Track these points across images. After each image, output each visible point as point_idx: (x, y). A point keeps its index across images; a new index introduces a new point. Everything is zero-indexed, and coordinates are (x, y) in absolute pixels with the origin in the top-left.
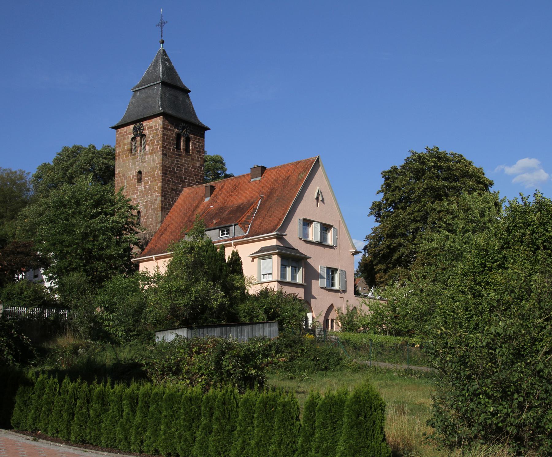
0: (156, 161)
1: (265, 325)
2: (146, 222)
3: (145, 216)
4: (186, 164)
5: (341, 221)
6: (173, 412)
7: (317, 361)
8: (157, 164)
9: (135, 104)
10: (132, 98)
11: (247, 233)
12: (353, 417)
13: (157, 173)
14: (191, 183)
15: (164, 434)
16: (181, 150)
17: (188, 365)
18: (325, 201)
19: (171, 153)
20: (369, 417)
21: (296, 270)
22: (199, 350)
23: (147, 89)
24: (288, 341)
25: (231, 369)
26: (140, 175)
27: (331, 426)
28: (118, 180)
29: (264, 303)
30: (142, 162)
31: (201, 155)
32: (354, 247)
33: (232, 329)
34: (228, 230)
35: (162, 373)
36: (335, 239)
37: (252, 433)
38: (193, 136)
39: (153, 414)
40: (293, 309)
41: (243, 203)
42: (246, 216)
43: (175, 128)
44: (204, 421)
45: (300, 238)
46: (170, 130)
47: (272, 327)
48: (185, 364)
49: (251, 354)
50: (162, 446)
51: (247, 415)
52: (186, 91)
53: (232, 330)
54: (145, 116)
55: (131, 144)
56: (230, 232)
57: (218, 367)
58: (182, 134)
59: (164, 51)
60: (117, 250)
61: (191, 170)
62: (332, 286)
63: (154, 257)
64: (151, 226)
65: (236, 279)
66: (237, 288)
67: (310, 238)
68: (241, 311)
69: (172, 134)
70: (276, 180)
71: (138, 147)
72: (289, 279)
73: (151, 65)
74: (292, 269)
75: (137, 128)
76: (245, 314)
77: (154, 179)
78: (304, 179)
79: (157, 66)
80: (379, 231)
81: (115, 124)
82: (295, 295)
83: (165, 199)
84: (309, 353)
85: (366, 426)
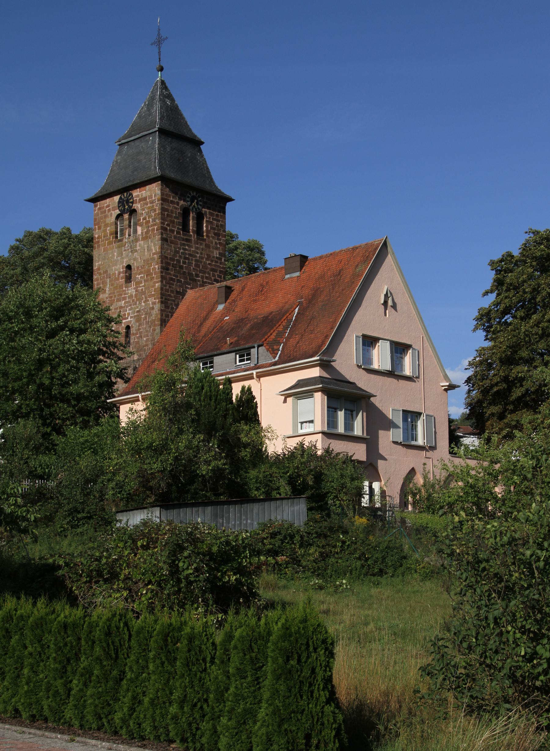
0: (152, 250)
1: (285, 502)
2: (138, 343)
3: (136, 334)
4: (198, 253)
5: (425, 338)
6: (42, 646)
7: (367, 560)
8: (154, 254)
9: (122, 164)
10: (117, 156)
11: (277, 359)
12: (280, 660)
13: (154, 269)
14: (206, 283)
15: (27, 683)
16: (189, 232)
17: (128, 566)
18: (398, 308)
19: (175, 237)
20: (306, 662)
21: (352, 415)
22: (148, 544)
23: (139, 140)
24: (321, 527)
25: (191, 574)
26: (129, 271)
27: (252, 676)
28: (97, 280)
29: (288, 467)
30: (132, 251)
31: (220, 240)
32: (446, 378)
33: (232, 508)
34: (249, 354)
35: (88, 579)
36: (417, 366)
37: (147, 684)
38: (208, 211)
39: (14, 650)
40: (342, 476)
41: (272, 312)
42: (276, 332)
43: (180, 199)
44: (84, 663)
45: (358, 366)
46: (172, 202)
47: (297, 505)
48: (124, 565)
49: (232, 548)
50: (23, 704)
51: (140, 653)
52: (197, 143)
53: (231, 510)
54: (135, 182)
55: (116, 224)
56: (252, 356)
57: (174, 570)
58: (191, 208)
59: (163, 82)
60: (88, 386)
61: (205, 263)
62: (412, 440)
63: (140, 396)
64: (146, 348)
65: (243, 430)
66: (246, 446)
67: (375, 366)
68: (251, 479)
69: (176, 208)
70: (322, 277)
71: (126, 229)
72: (341, 429)
73: (145, 105)
74: (345, 413)
75: (124, 201)
76: (258, 485)
77: (149, 278)
78: (363, 273)
79: (152, 106)
80: (488, 354)
81: (91, 195)
82: (350, 454)
83: (166, 307)
84: (354, 546)
85: (299, 676)
